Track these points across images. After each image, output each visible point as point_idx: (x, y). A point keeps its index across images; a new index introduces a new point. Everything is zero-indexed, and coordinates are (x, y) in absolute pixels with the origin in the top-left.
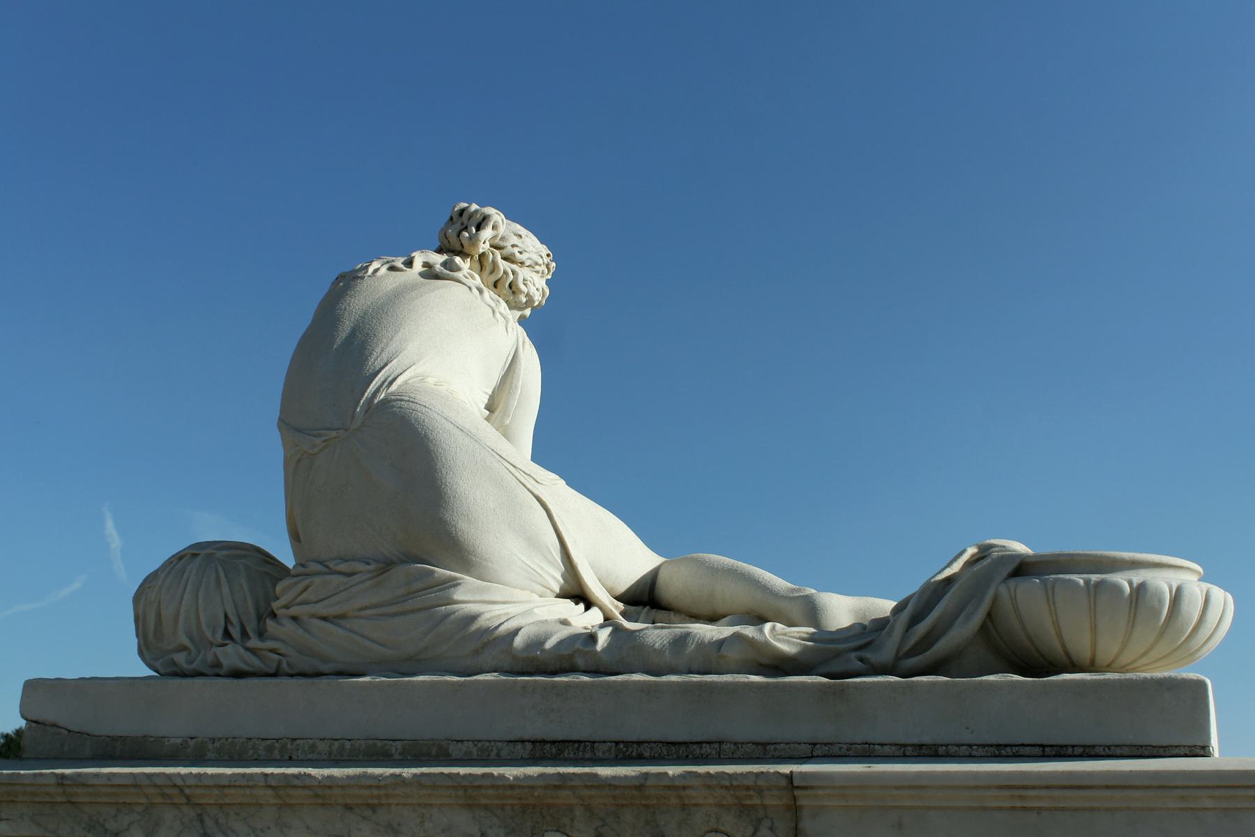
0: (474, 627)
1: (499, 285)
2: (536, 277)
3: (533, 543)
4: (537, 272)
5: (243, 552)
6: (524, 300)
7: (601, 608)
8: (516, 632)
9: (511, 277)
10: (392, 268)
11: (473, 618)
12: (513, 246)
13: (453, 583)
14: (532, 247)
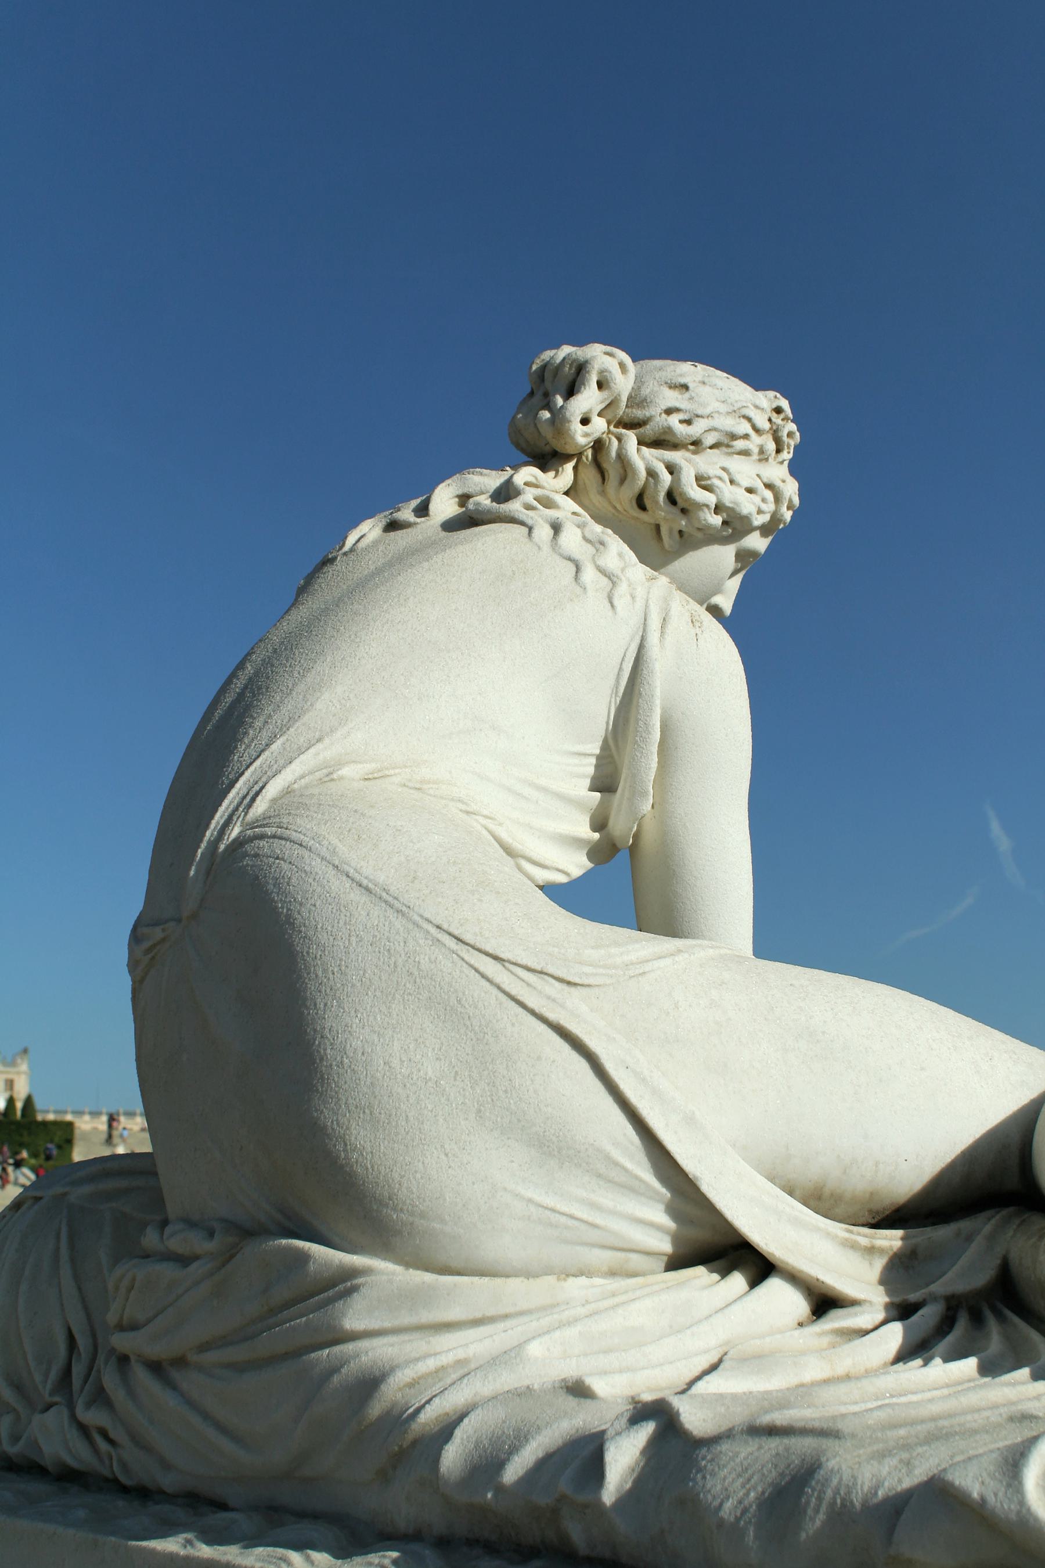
0: (375, 1409)
1: (647, 502)
2: (746, 470)
3: (554, 1148)
4: (745, 453)
5: (123, 1183)
6: (716, 520)
7: (794, 1278)
8: (446, 1431)
9: (666, 478)
10: (393, 526)
11: (371, 1383)
12: (669, 411)
13: (342, 1284)
14: (716, 398)
